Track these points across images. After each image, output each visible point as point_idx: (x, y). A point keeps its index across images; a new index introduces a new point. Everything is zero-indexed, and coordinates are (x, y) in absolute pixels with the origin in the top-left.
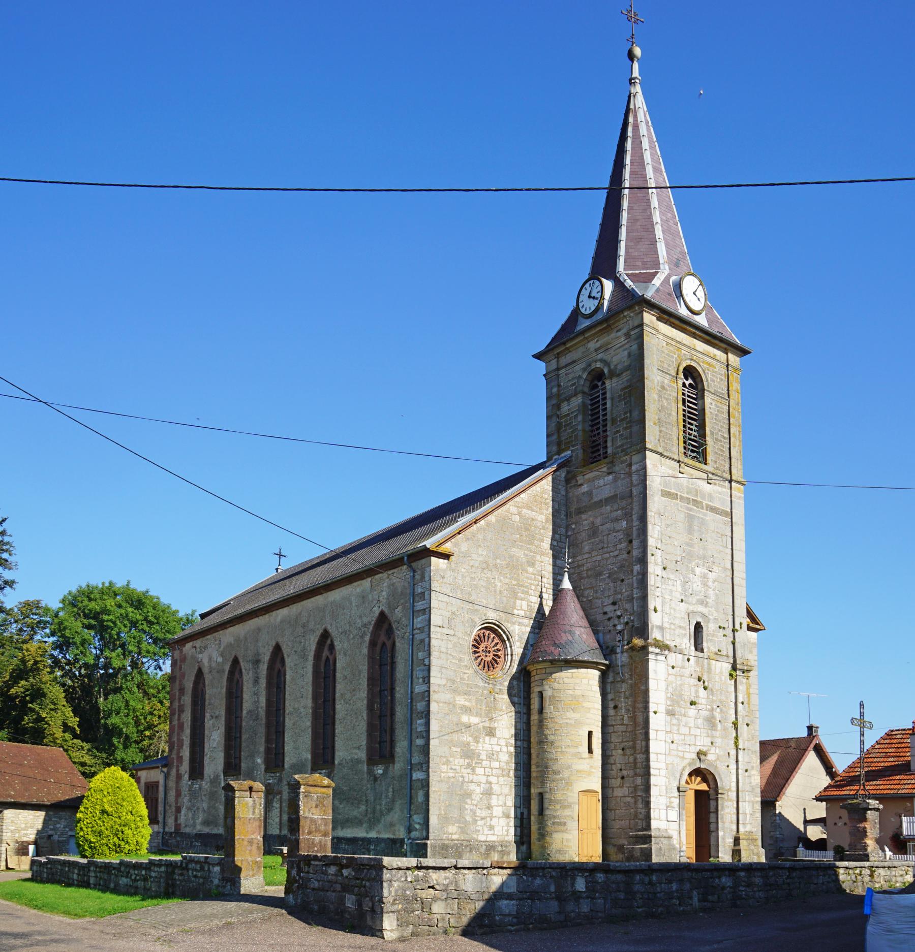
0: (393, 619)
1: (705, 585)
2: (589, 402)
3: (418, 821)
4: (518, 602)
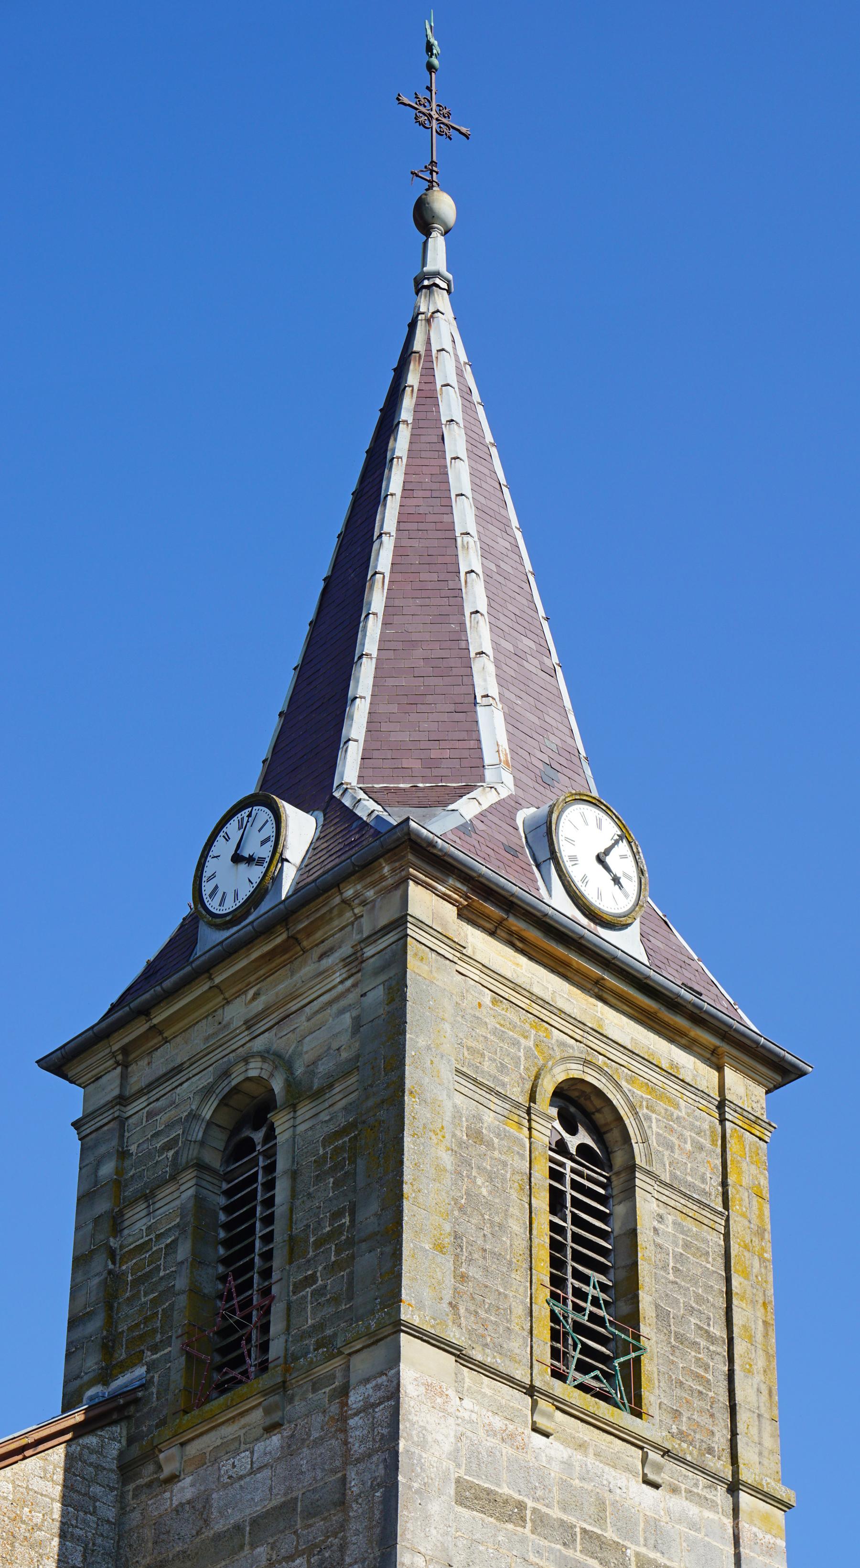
2: (223, 1201)
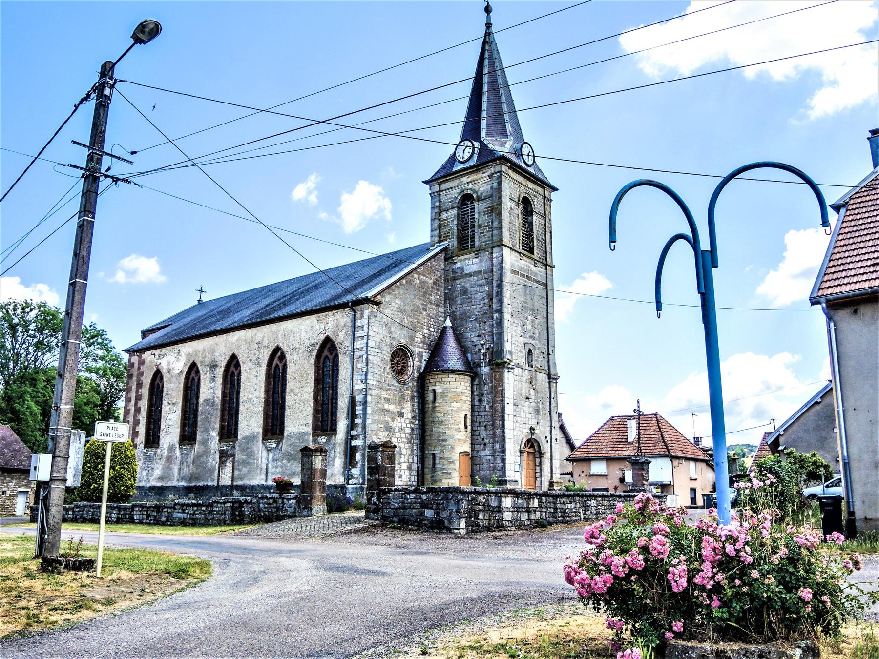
0: (337, 341)
1: (533, 326)
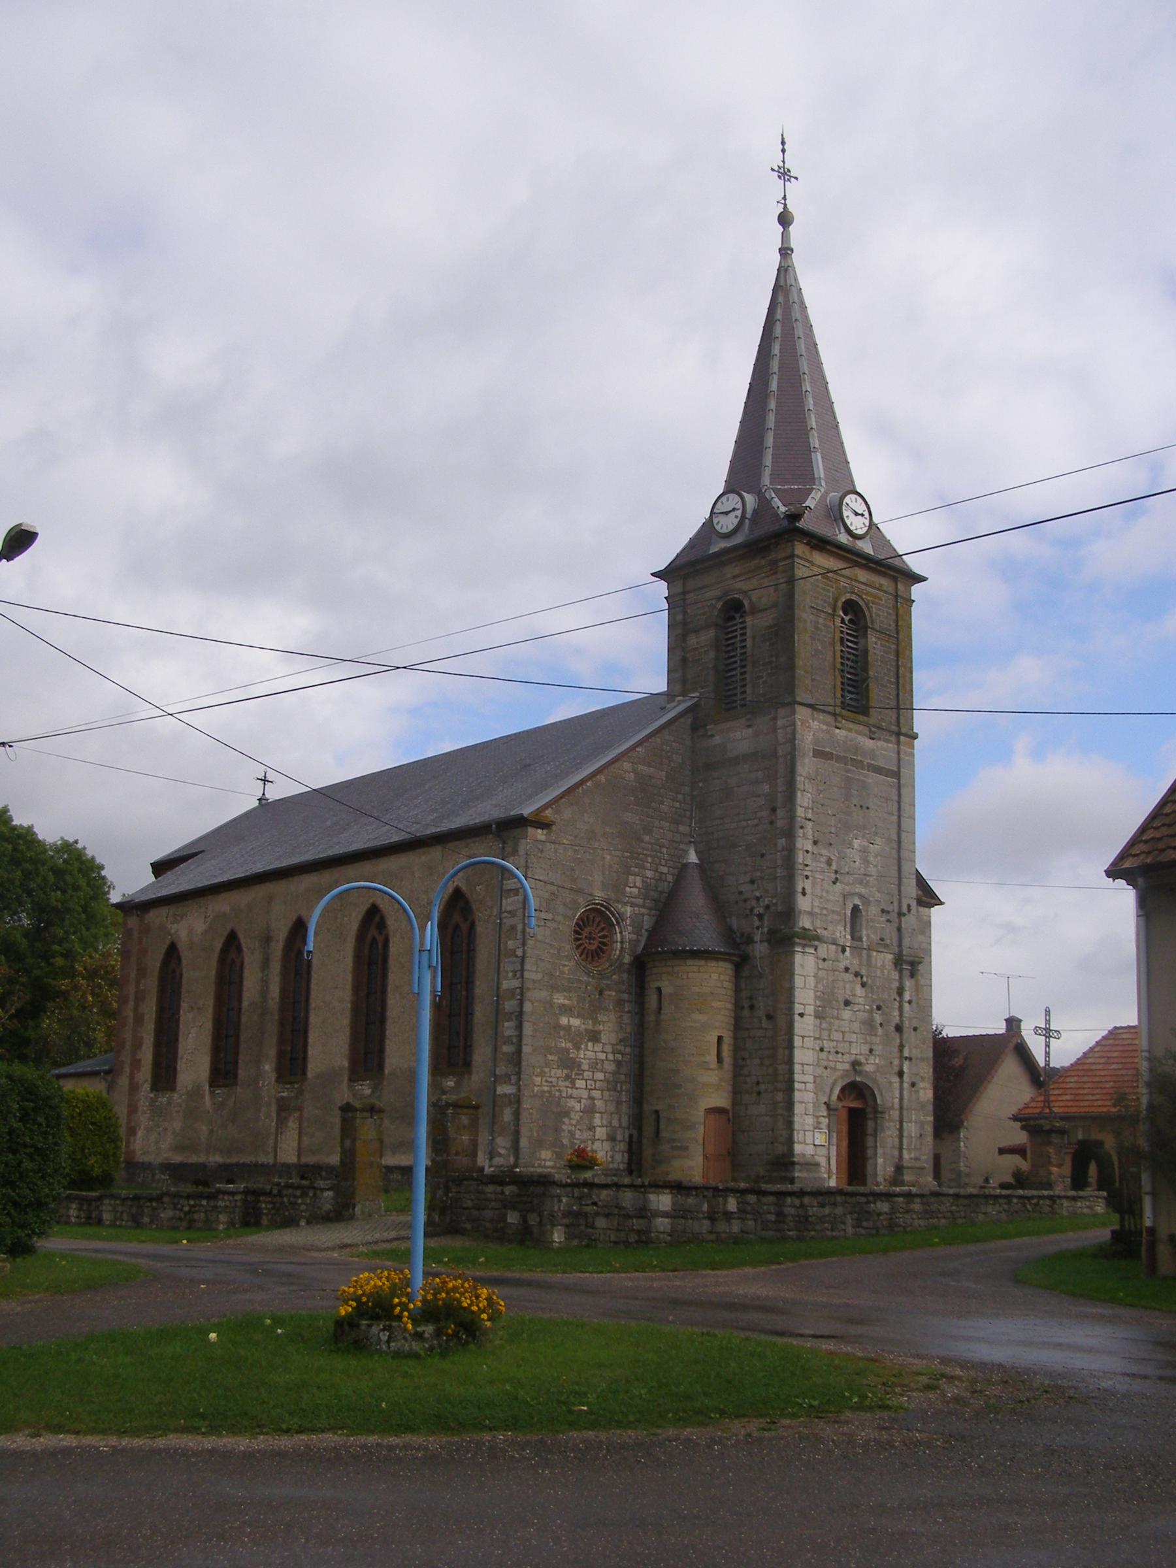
1: (866, 861)
3: (503, 1144)
4: (631, 878)
